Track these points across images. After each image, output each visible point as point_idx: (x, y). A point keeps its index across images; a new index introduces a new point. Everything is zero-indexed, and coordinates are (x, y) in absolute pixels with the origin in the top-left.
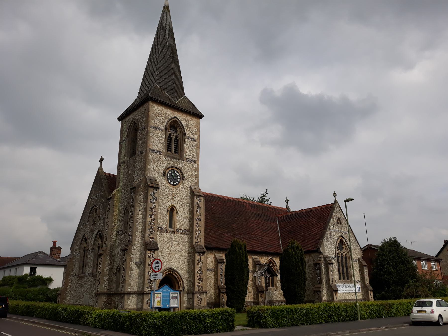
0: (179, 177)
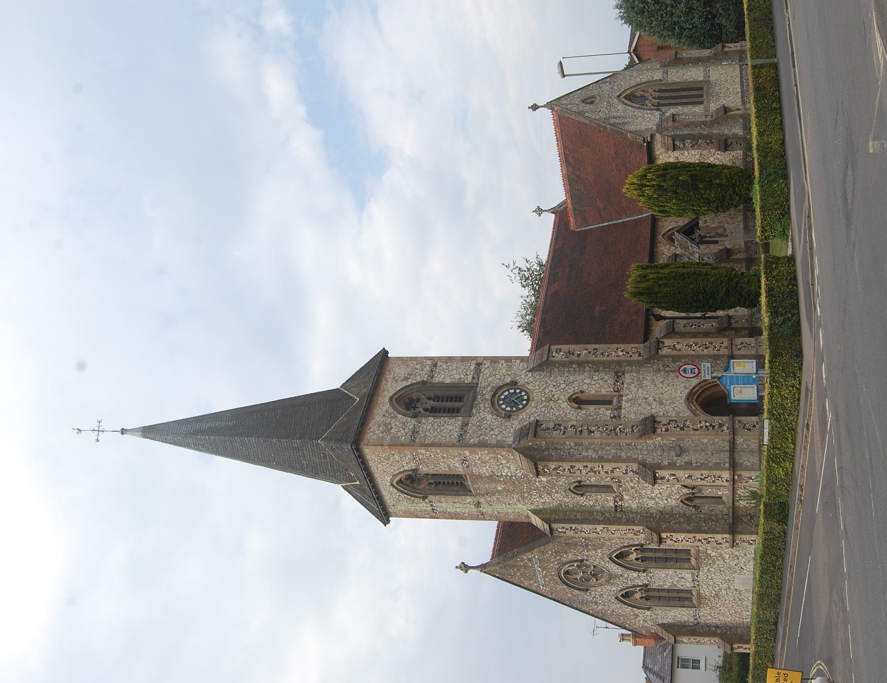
0: (512, 391)
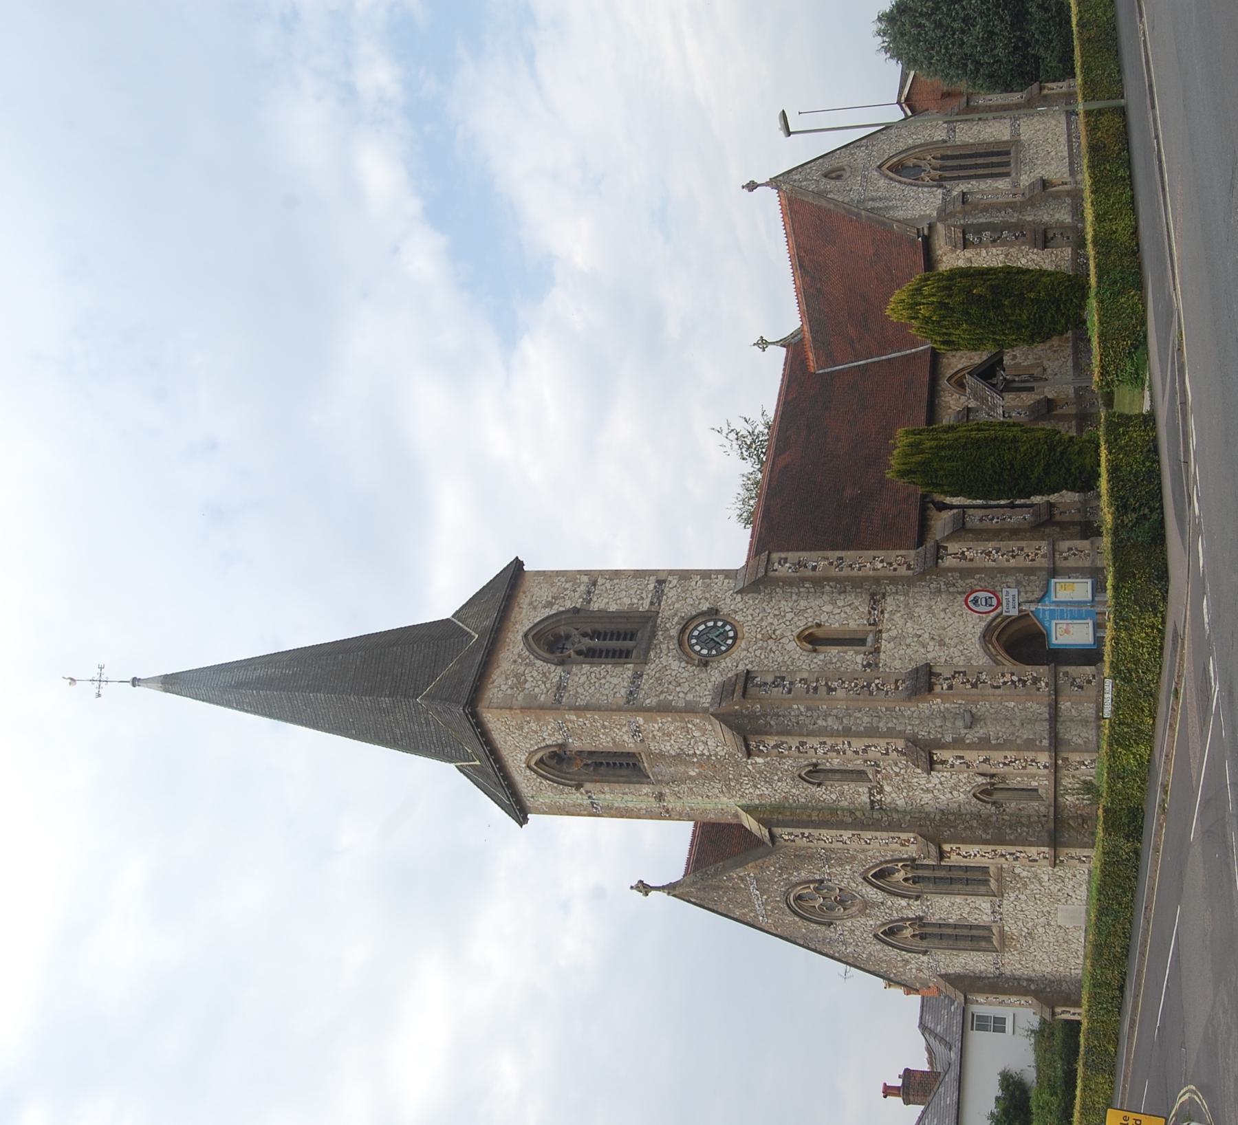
0: (711, 624)
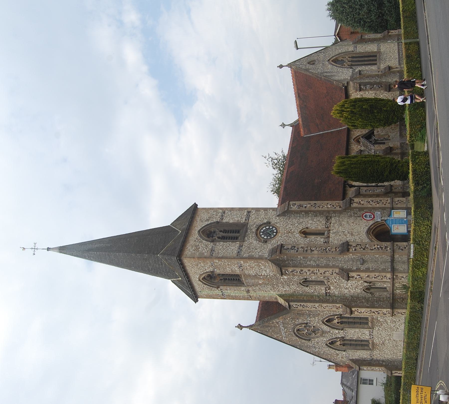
0: (268, 227)
